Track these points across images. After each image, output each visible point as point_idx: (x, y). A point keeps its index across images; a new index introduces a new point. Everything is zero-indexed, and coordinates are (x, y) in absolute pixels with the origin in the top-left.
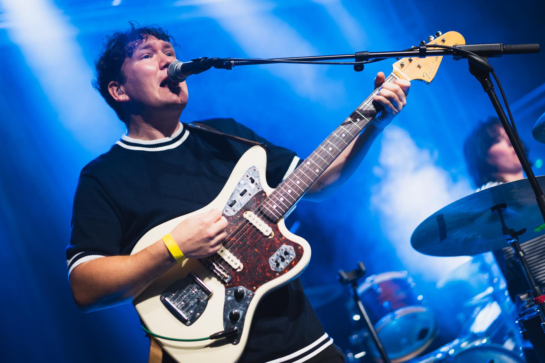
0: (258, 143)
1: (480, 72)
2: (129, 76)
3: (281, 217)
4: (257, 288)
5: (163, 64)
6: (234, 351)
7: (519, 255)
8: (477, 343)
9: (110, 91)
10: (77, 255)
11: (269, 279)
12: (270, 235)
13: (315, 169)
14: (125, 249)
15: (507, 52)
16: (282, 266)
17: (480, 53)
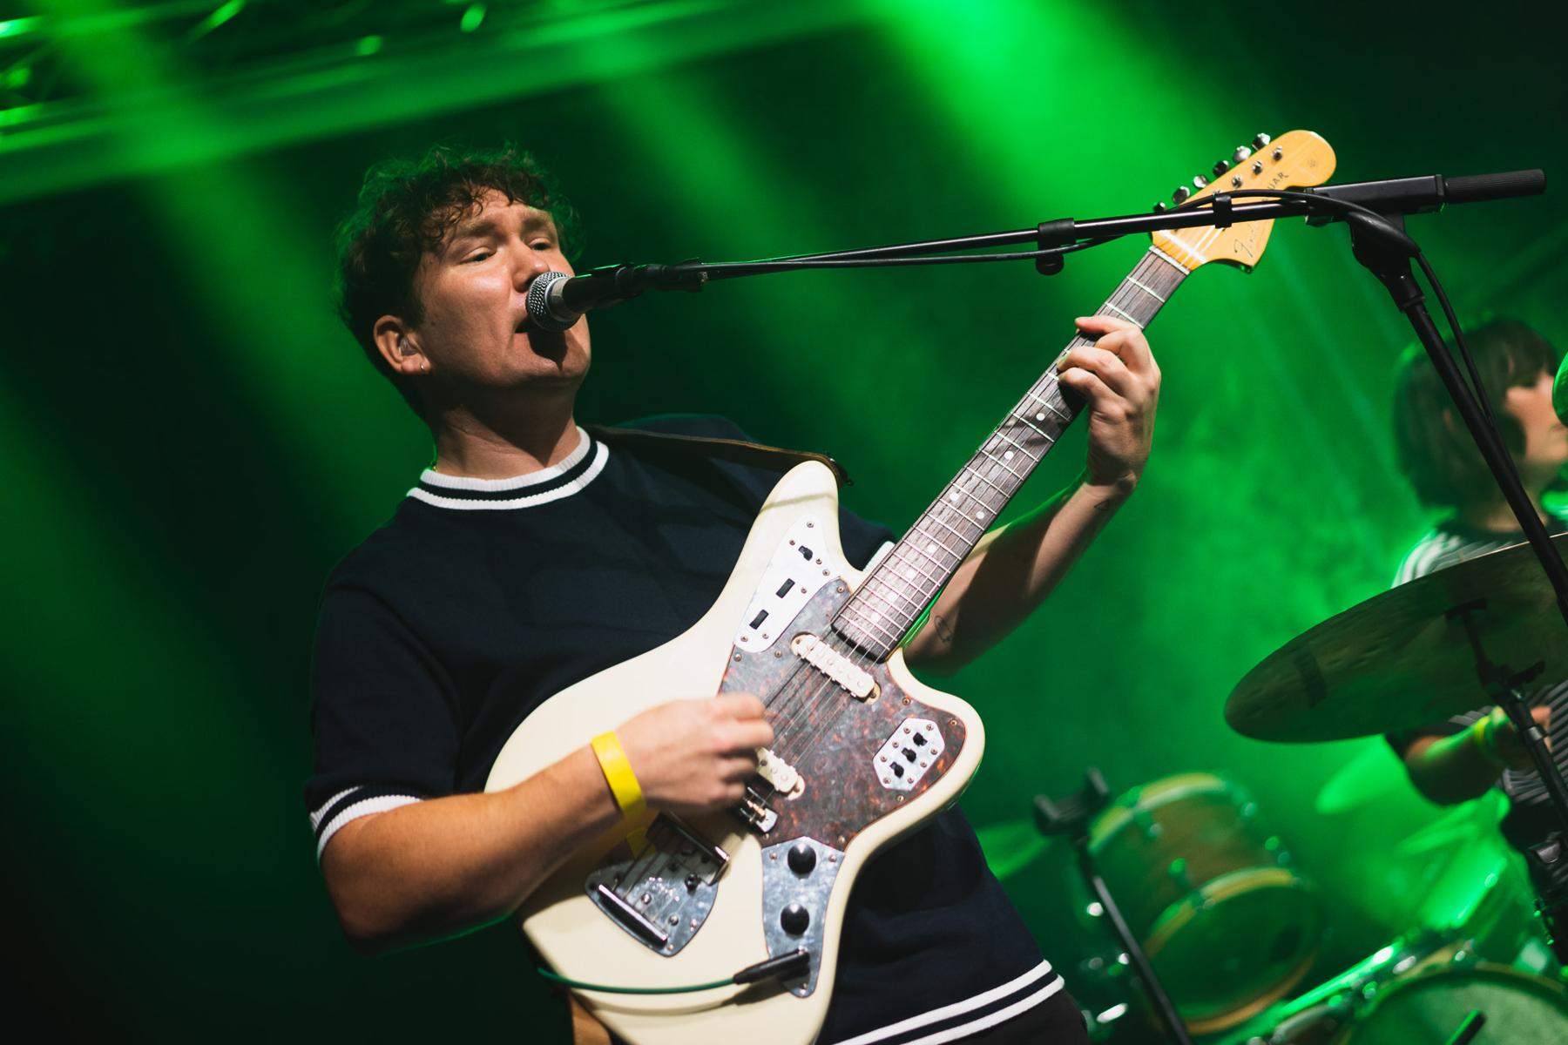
0: (810, 454)
1: (1385, 259)
2: (430, 306)
3: (894, 646)
4: (848, 840)
5: (523, 276)
6: (805, 1010)
7: (1530, 736)
8: (1441, 958)
9: (382, 347)
10: (347, 792)
11: (880, 815)
12: (871, 694)
13: (972, 511)
14: (466, 772)
15: (1454, 197)
16: (914, 772)
17: (1380, 205)
